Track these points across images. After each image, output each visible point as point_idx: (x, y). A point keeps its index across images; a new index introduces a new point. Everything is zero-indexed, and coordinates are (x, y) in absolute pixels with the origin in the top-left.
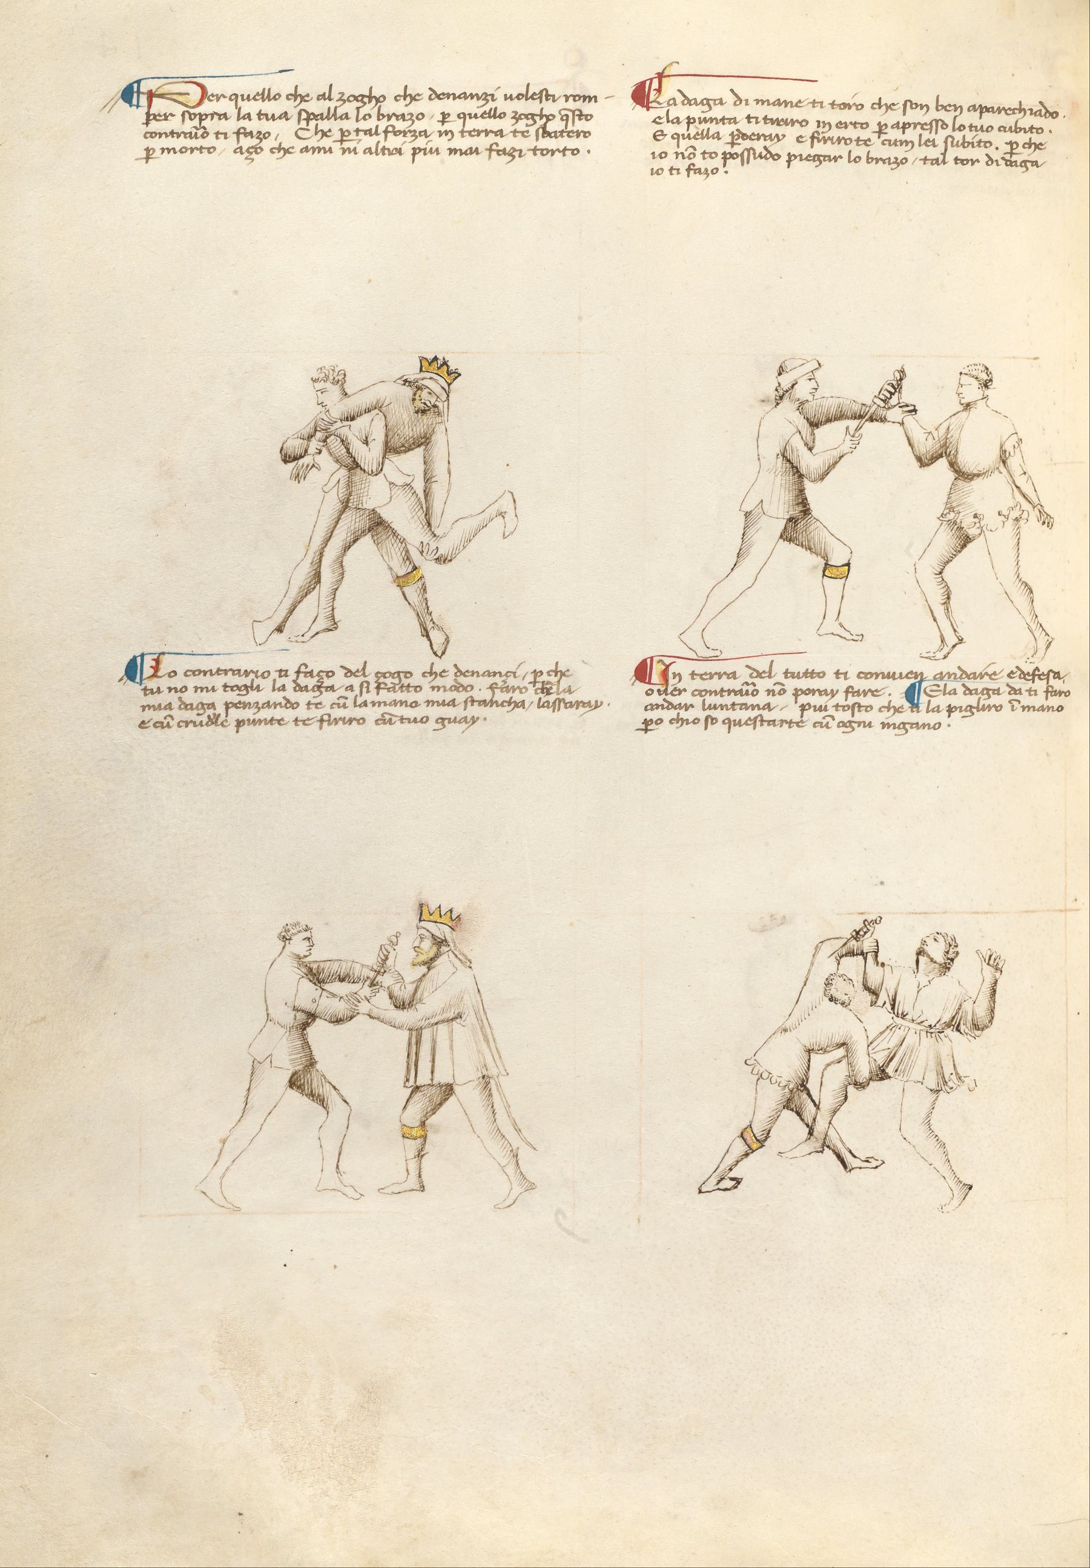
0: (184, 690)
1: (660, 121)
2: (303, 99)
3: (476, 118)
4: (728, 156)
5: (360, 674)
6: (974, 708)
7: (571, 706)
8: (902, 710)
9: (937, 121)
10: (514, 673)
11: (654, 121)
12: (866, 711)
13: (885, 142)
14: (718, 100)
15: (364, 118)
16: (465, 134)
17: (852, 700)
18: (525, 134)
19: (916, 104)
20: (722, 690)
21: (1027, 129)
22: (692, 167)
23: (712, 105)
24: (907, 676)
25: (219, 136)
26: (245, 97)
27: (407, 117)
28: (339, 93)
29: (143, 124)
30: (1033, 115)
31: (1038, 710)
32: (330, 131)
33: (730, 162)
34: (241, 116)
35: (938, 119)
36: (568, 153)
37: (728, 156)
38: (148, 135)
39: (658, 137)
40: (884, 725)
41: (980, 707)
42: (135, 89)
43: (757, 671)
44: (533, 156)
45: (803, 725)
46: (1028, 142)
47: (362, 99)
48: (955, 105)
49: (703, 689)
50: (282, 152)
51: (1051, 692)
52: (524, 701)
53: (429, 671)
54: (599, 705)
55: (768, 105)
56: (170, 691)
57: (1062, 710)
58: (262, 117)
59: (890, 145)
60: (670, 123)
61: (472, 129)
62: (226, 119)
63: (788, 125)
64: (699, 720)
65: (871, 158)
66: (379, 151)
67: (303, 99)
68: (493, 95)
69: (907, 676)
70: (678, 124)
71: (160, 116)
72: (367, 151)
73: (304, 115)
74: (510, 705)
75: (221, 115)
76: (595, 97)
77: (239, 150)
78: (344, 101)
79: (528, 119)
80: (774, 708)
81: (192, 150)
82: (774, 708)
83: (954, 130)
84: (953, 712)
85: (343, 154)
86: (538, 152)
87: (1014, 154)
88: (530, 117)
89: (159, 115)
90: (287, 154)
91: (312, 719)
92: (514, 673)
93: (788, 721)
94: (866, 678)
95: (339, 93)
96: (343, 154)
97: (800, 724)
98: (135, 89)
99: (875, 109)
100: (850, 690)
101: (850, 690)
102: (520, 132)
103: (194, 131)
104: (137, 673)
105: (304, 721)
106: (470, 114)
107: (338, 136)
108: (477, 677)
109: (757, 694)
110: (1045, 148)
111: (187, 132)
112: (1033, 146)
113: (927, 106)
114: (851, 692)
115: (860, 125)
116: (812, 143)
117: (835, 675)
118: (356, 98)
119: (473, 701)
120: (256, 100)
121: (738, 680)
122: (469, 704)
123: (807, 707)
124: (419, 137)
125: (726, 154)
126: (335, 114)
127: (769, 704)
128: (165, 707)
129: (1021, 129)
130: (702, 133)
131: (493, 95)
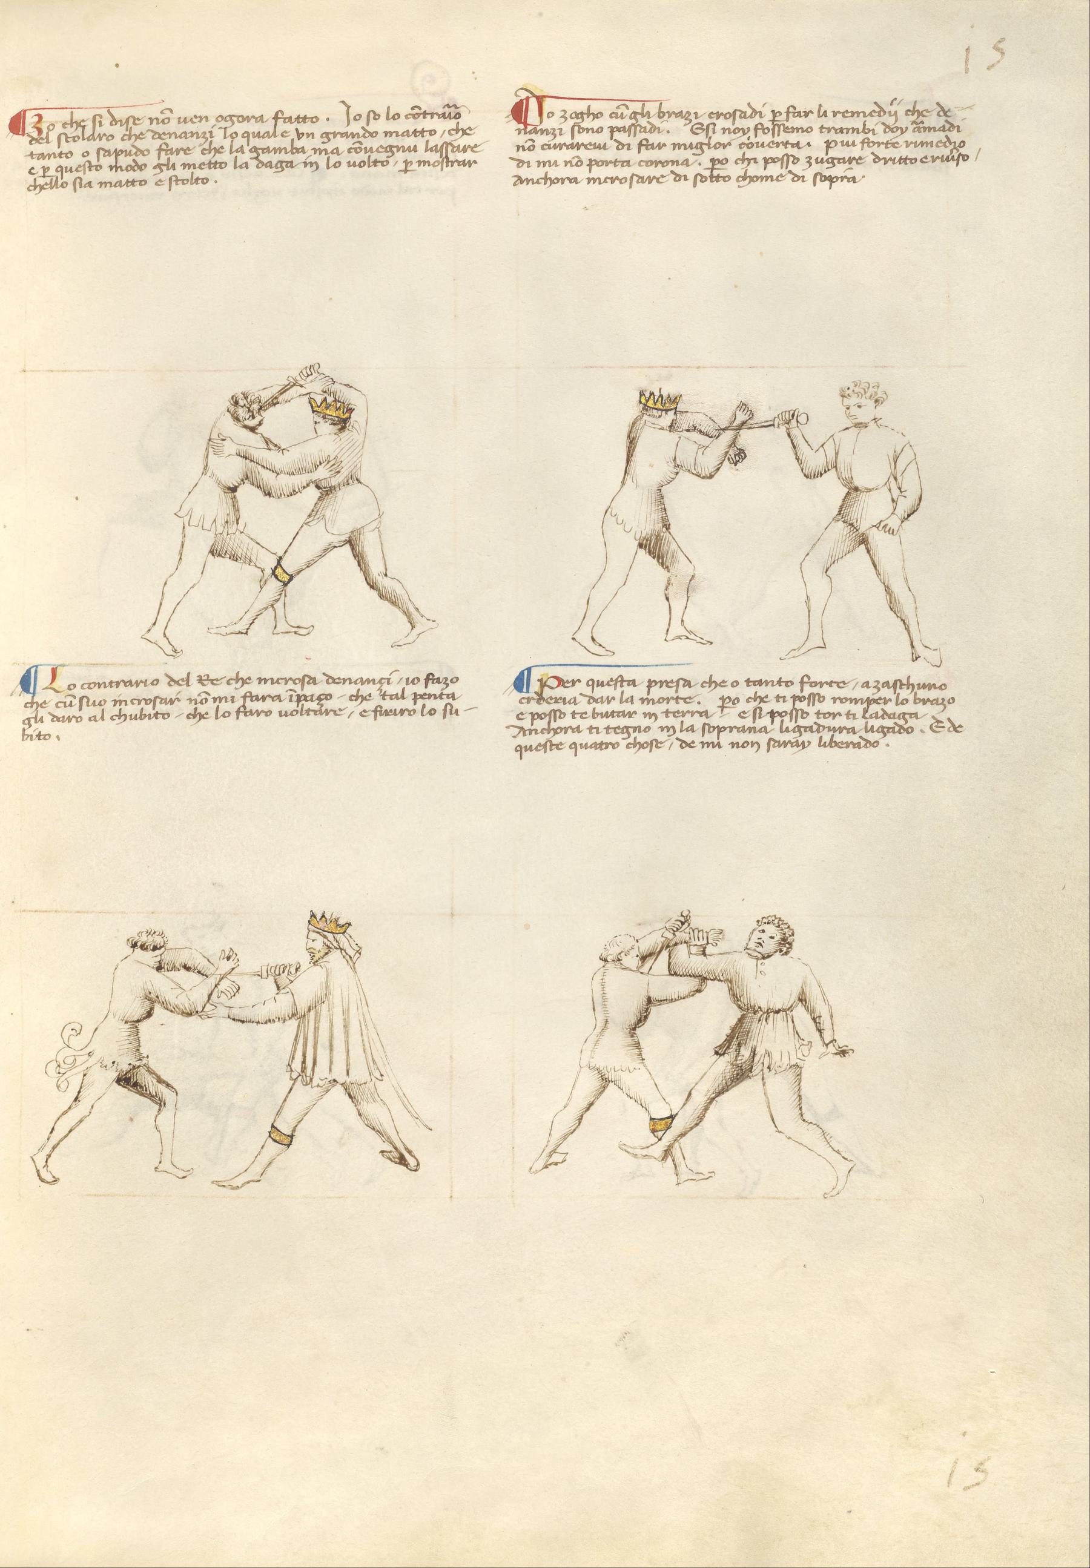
1: (744, 716)
2: (244, 682)
6: (639, 114)
7: (252, 714)
8: (586, 716)
10: (389, 680)
11: (739, 715)
13: (114, 718)
17: (808, 690)
19: (713, 727)
21: (437, 696)
31: (115, 186)
32: (207, 713)
36: (671, 715)
37: (536, 717)
43: (332, 678)
45: (162, 183)
46: (355, 694)
50: (240, 682)
54: (904, 131)
57: (964, 145)
61: (676, 710)
64: (229, 713)
65: (868, 129)
67: (244, 682)
74: (466, 151)
76: (281, 715)
80: (701, 116)
82: (701, 116)
84: (834, 182)
85: (305, 167)
86: (200, 181)
88: (228, 119)
90: (43, 190)
92: (389, 680)
93: (613, 161)
94: (647, 166)
96: (305, 167)
101: (431, 677)
102: (672, 713)
104: (523, 685)
109: (823, 701)
114: (164, 150)
117: (816, 715)
119: (177, 180)
122: (174, 183)
123: (833, 144)
125: (417, 695)
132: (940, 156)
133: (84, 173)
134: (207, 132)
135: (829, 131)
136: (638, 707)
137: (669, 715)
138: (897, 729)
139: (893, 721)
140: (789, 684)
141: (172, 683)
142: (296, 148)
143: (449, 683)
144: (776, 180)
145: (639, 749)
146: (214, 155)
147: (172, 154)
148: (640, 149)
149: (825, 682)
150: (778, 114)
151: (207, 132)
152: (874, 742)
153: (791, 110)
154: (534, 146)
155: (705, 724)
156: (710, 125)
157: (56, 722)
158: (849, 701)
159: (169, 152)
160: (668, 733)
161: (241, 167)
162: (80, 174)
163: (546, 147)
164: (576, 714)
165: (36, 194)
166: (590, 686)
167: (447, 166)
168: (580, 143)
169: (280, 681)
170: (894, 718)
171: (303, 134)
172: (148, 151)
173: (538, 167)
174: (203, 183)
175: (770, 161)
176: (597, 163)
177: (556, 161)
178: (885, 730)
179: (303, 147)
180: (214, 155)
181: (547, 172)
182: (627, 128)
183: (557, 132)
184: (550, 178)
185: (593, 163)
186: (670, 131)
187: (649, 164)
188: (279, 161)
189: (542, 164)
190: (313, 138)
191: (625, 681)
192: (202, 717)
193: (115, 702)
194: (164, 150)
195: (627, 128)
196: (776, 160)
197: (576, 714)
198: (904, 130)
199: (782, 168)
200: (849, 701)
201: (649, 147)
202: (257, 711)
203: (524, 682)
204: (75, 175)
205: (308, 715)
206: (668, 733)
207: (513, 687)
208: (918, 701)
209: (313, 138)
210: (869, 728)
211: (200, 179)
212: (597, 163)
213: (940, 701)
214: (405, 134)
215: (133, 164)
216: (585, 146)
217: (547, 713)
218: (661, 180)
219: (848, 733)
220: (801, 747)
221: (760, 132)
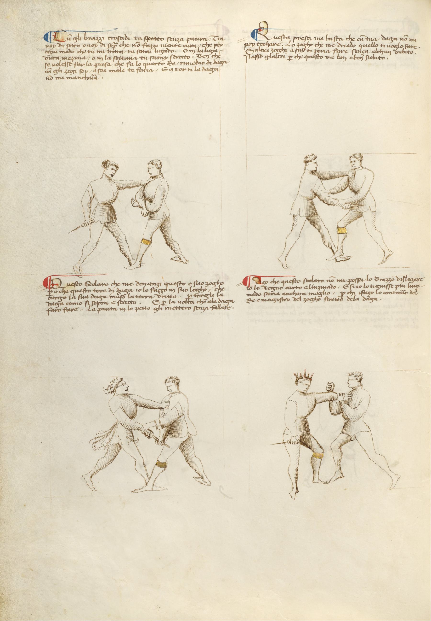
3: (367, 294)
4: (317, 51)
5: (352, 58)
22: (145, 44)
23: (393, 40)
25: (309, 51)
27: (386, 280)
29: (114, 281)
37: (317, 51)
39: (155, 303)
41: (325, 293)
42: (256, 32)
44: (307, 52)
47: (56, 71)
49: (180, 68)
51: (140, 70)
52: (172, 68)
55: (403, 40)
59: (360, 40)
60: (376, 57)
62: (123, 53)
63: (54, 311)
65: (404, 52)
66: (277, 57)
70: (172, 285)
72: (171, 70)
75: (122, 38)
79: (71, 72)
81: (186, 308)
83: (364, 288)
90: (83, 53)
99: (116, 66)
103: (92, 76)
106: (148, 64)
108: (364, 45)
112: (216, 57)
113: (390, 52)
115: (133, 303)
116: (212, 309)
118: (212, 284)
120: (369, 47)
121: (153, 71)
126: (163, 427)
127: (84, 57)
128: (94, 78)
129: (375, 58)
130: (372, 45)
133: (83, 293)
134: (251, 58)
136: (108, 300)
140: (322, 57)
142: (339, 57)
145: (299, 58)
147: (339, 52)
150: (291, 57)
151: (251, 58)
152: (283, 283)
153: (363, 291)
154: (139, 45)
159: (338, 52)
162: (82, 293)
164: (380, 58)
166: (306, 58)
173: (309, 295)
174: (188, 58)
175: (351, 281)
176: (139, 309)
177: (416, 39)
178: (413, 280)
179: (131, 289)
181: (106, 55)
182: (386, 286)
183: (159, 284)
184: (351, 38)
185: (189, 39)
187: (98, 291)
188: (391, 38)
189: (311, 294)
191: (87, 290)
192: (300, 57)
194: (66, 310)
195: (386, 286)
196: (354, 281)
197: (380, 58)
198: (55, 46)
204: (79, 293)
205: (188, 303)
208: (355, 58)
210: (156, 51)
211: (130, 51)
212: (139, 309)
213: (96, 38)
214: (269, 300)
219: (56, 59)
220: (164, 59)
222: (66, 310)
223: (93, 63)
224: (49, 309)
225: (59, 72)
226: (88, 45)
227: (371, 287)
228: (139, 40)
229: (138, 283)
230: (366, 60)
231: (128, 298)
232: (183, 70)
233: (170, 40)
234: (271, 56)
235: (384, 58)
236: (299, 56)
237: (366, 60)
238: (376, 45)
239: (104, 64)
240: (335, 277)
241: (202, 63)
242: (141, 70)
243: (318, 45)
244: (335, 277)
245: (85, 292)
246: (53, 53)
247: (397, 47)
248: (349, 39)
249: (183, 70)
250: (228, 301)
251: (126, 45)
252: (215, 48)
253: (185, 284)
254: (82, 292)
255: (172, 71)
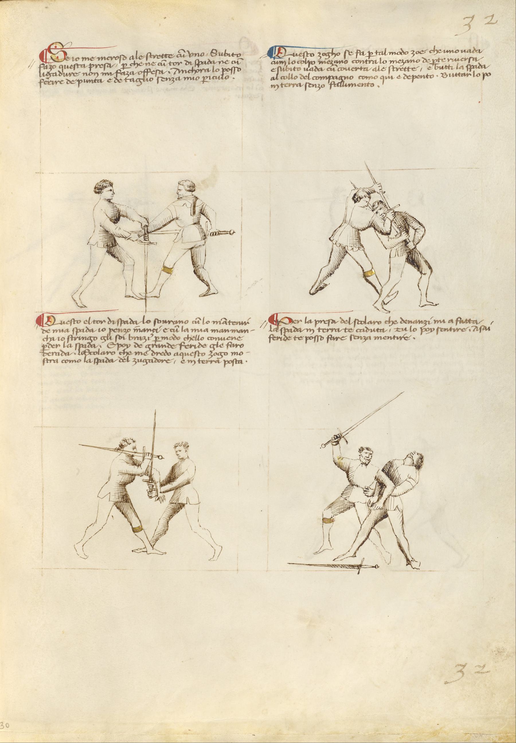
0: (186, 322)
9: (235, 68)
12: (431, 78)
14: (362, 329)
15: (147, 322)
16: (296, 339)
18: (350, 330)
20: (394, 337)
24: (227, 339)
26: (451, 75)
28: (133, 359)
30: (184, 332)
33: (308, 341)
34: (307, 321)
35: (235, 67)
38: (314, 78)
40: (375, 338)
48: (409, 321)
51: (231, 345)
53: (118, 74)
56: (390, 54)
58: (296, 339)
65: (227, 53)
68: (429, 322)
69: (227, 339)
71: (86, 321)
73: (75, 330)
77: (461, 67)
78: (404, 63)
87: (205, 81)
89: (204, 361)
90: (65, 60)
91: (345, 337)
95: (133, 359)
97: (300, 338)
98: (275, 319)
100: (42, 81)
105: (299, 338)
107: (368, 54)
110: (416, 70)
111: (371, 269)
116: (227, 347)
124: (321, 88)
131: (429, 322)
132: (73, 65)
135: (195, 330)
137: (320, 330)
138: (293, 329)
139: (197, 342)
141: (342, 322)
143: (415, 54)
144: (237, 339)
146: (190, 341)
148: (227, 347)
149: (329, 329)
150: (371, 54)
155: (351, 335)
156: (106, 64)
157: (310, 323)
158: (215, 339)
160: (389, 324)
161: (308, 322)
163: (329, 69)
165: (136, 68)
167: (74, 323)
168: (88, 80)
169: (109, 58)
170: (198, 340)
171: (193, 54)
172: (170, 354)
175: (308, 338)
180: (190, 341)
186: (234, 78)
190: (248, 332)
193: (192, 330)
198: (129, 346)
199: (76, 349)
200: (215, 339)
201: (232, 346)
202: (419, 321)
203: (273, 51)
206: (389, 324)
207: (267, 321)
209: (248, 332)
215: (174, 337)
216: (161, 354)
217: (314, 337)
218: (62, 82)
221: (183, 348)
222: (119, 73)
223: (209, 343)
224: (228, 343)
225: (144, 81)
226: (60, 330)
227: (295, 340)
228: (119, 332)
229: (403, 320)
230: (270, 342)
231: (84, 362)
232: (350, 571)
233: (441, 331)
234: (218, 344)
235: (158, 65)
236: (392, 321)
237: (270, 342)
238: (414, 329)
239: (102, 65)
240: (347, 336)
241: (350, 77)
242: (232, 345)
243: (389, 322)
244: (347, 336)
245: (139, 360)
246: (345, 79)
247: (106, 338)
248: (389, 322)
249: (350, 571)
250: (90, 338)
251: (138, 65)
252: (309, 74)
253: (381, 322)
254: (328, 324)
255: (207, 332)
